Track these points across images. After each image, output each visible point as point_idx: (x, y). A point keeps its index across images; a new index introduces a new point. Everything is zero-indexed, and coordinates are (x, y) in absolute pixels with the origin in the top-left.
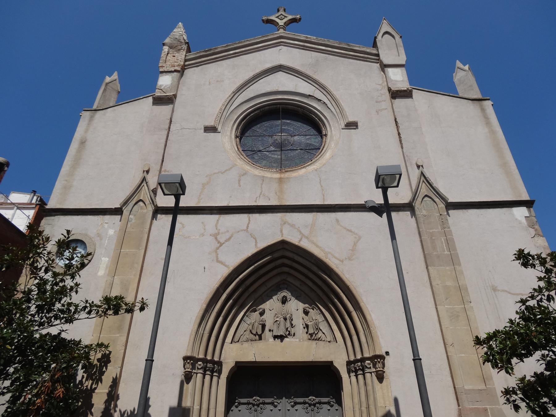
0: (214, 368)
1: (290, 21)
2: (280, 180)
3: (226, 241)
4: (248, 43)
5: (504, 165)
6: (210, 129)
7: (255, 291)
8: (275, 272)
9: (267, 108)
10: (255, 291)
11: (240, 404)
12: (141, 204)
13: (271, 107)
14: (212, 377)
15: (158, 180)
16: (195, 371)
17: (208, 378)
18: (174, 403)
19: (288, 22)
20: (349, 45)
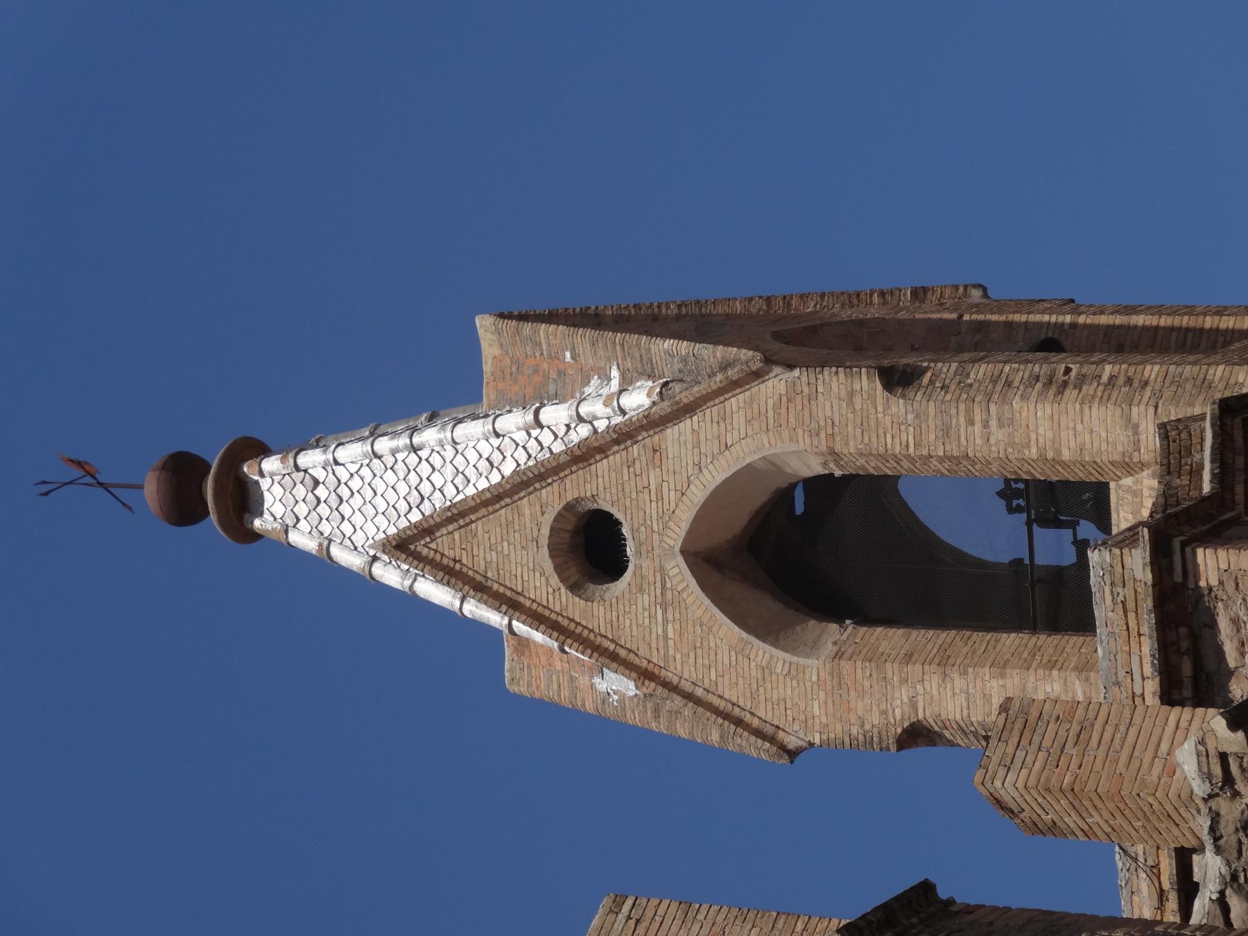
15: (459, 515)
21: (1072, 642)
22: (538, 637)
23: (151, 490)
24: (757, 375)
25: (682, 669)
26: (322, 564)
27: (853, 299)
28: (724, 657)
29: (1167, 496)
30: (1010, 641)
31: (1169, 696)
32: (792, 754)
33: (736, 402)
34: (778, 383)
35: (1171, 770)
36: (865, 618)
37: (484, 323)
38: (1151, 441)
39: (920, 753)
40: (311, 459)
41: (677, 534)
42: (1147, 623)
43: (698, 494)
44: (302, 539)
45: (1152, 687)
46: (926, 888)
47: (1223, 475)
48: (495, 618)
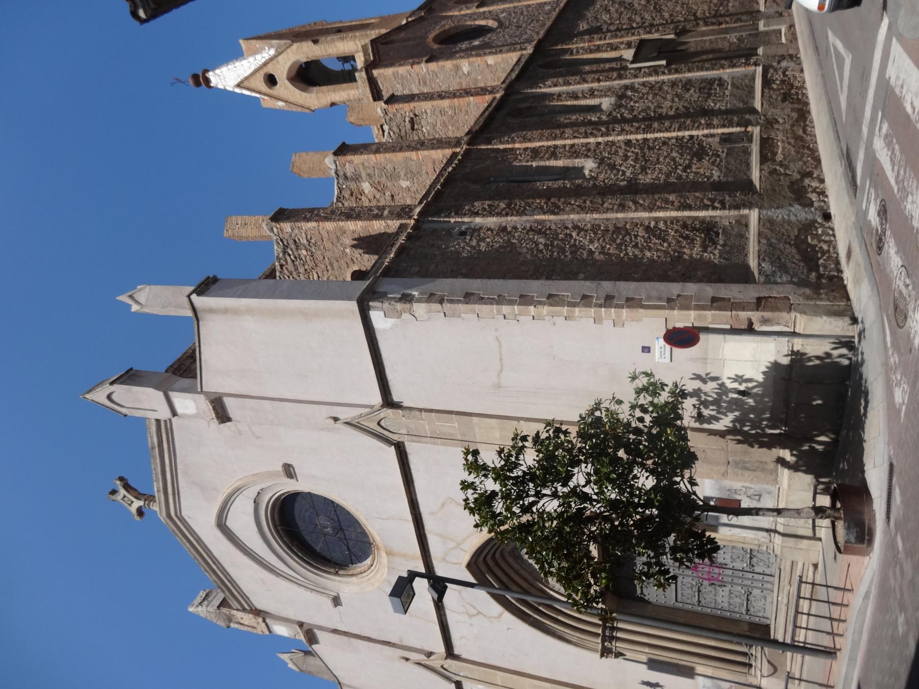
0: (609, 627)
1: (129, 489)
2: (389, 553)
3: (475, 609)
4: (192, 550)
5: (305, 315)
6: (336, 601)
7: (526, 580)
8: (503, 565)
9: (285, 539)
10: (526, 580)
11: (642, 593)
12: (382, 423)
13: (283, 536)
14: (619, 639)
15: (247, 78)
16: (614, 648)
17: (620, 635)
18: (645, 667)
19: (132, 492)
20: (153, 448)
21: (354, 84)
22: (266, 98)
23: (191, 82)
24: (291, 45)
25: (292, 99)
26: (225, 91)
27: (304, 26)
28: (298, 96)
29: (366, 61)
30: (344, 85)
31: (375, 100)
32: (313, 111)
33: (289, 50)
34: (295, 46)
35: (377, 113)
36: (320, 85)
37: (241, 41)
38: (360, 48)
39: (334, 107)
40: (217, 71)
41: (285, 76)
42: (367, 84)
43: (287, 68)
44: (221, 87)
45: (371, 99)
46: (344, 143)
47: (374, 56)
48: (257, 95)
